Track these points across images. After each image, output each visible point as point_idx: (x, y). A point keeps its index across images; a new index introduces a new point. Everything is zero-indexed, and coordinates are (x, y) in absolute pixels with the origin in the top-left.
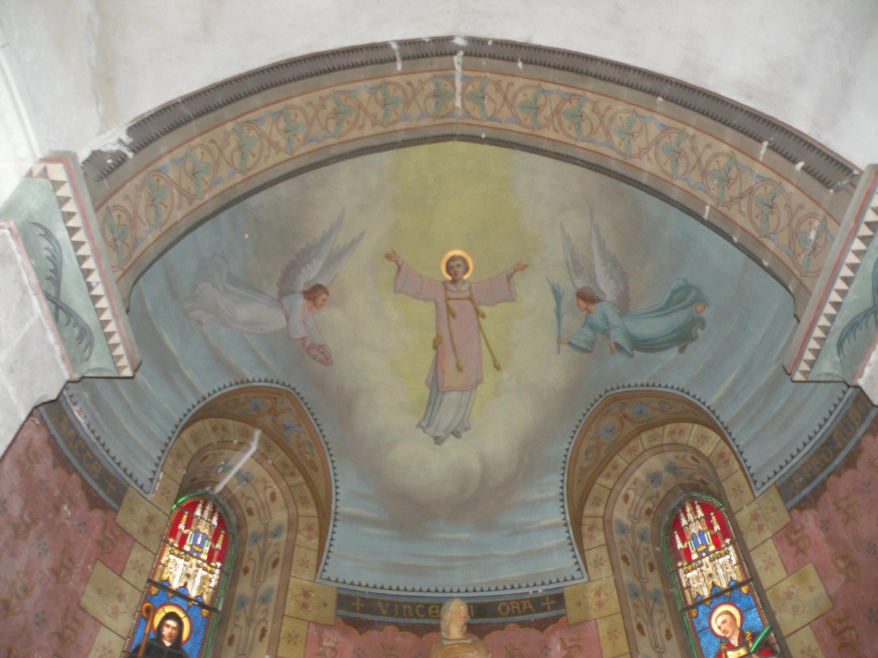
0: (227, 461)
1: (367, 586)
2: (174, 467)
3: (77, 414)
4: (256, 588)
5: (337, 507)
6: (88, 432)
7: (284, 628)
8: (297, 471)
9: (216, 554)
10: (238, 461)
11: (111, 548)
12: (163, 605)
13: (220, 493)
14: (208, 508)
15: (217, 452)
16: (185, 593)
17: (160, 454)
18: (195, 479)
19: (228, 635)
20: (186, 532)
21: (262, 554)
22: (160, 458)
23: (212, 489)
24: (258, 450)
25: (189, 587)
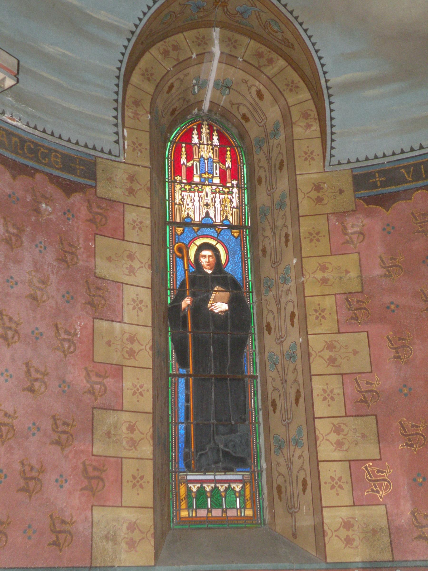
0: (198, 78)
1: (384, 156)
2: (136, 116)
3: (9, 121)
4: (270, 195)
5: (327, 81)
6: (31, 131)
7: (302, 229)
8: (275, 56)
9: (228, 173)
10: (208, 73)
11: (104, 220)
12: (192, 241)
13: (210, 111)
14: (205, 130)
15: (181, 75)
16: (210, 221)
17: (114, 113)
18: (174, 111)
19: (261, 248)
20: (189, 164)
21: (269, 159)
22: (116, 117)
23: (200, 109)
24: (222, 53)
25: (212, 215)
